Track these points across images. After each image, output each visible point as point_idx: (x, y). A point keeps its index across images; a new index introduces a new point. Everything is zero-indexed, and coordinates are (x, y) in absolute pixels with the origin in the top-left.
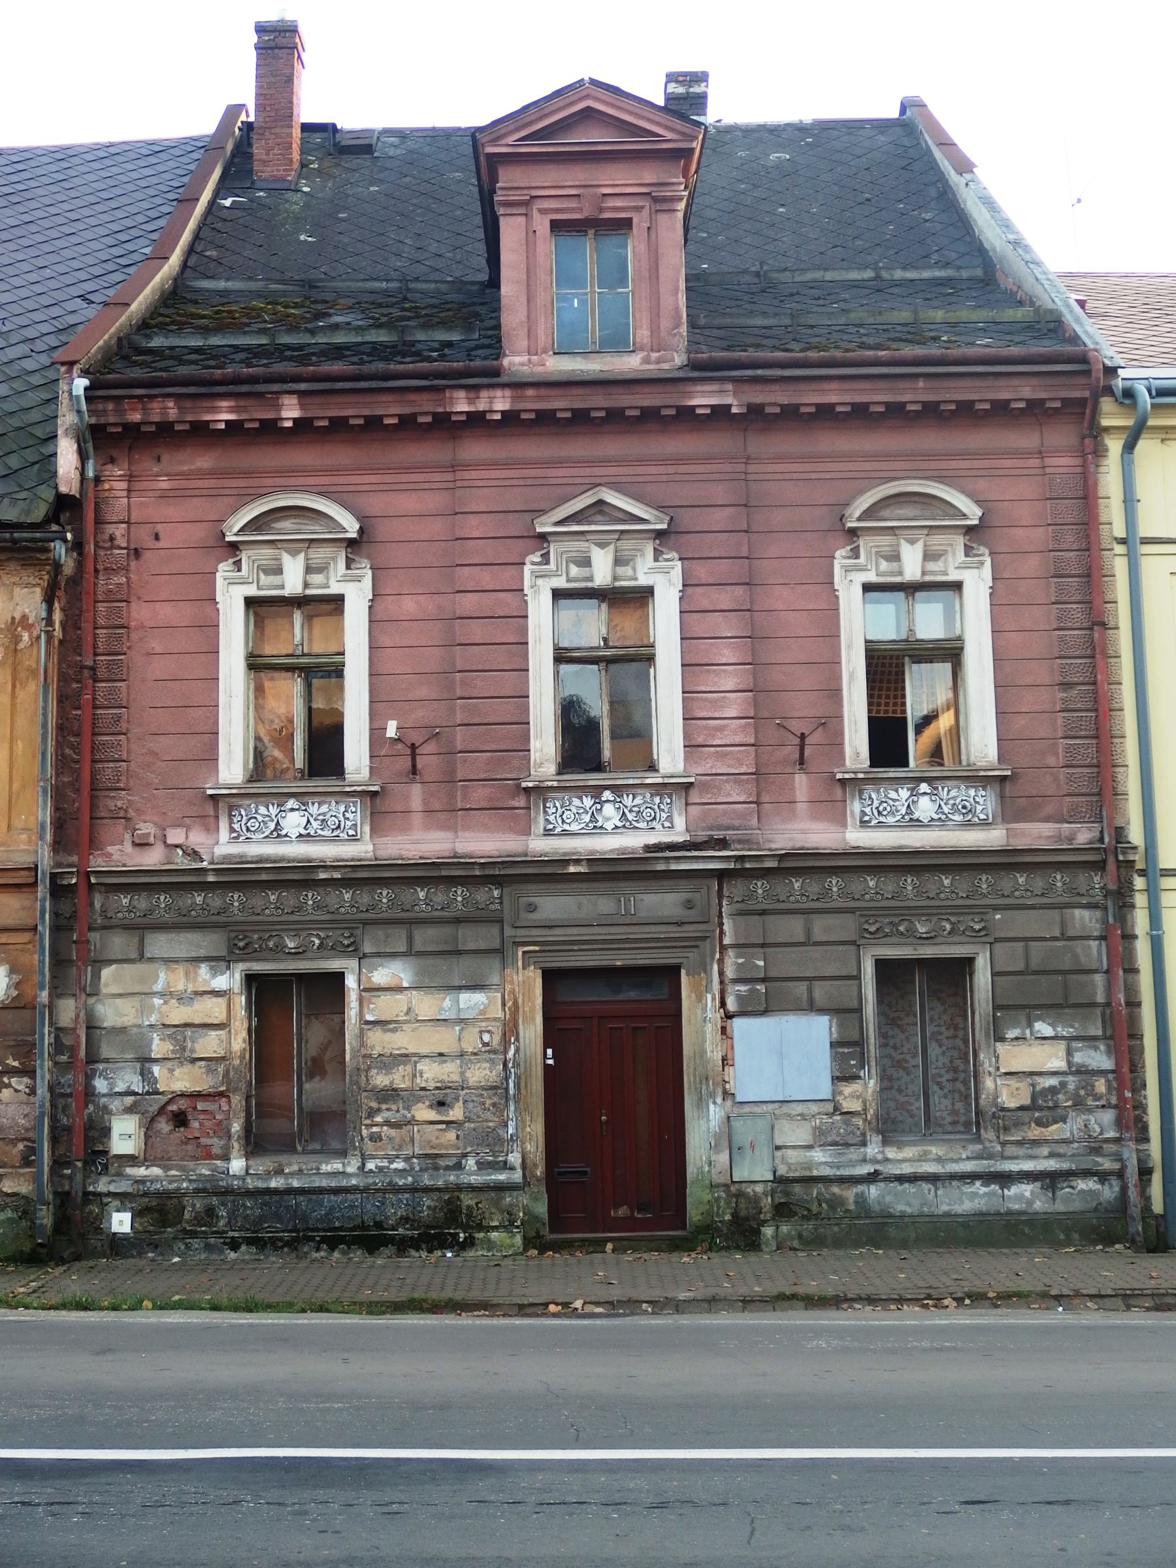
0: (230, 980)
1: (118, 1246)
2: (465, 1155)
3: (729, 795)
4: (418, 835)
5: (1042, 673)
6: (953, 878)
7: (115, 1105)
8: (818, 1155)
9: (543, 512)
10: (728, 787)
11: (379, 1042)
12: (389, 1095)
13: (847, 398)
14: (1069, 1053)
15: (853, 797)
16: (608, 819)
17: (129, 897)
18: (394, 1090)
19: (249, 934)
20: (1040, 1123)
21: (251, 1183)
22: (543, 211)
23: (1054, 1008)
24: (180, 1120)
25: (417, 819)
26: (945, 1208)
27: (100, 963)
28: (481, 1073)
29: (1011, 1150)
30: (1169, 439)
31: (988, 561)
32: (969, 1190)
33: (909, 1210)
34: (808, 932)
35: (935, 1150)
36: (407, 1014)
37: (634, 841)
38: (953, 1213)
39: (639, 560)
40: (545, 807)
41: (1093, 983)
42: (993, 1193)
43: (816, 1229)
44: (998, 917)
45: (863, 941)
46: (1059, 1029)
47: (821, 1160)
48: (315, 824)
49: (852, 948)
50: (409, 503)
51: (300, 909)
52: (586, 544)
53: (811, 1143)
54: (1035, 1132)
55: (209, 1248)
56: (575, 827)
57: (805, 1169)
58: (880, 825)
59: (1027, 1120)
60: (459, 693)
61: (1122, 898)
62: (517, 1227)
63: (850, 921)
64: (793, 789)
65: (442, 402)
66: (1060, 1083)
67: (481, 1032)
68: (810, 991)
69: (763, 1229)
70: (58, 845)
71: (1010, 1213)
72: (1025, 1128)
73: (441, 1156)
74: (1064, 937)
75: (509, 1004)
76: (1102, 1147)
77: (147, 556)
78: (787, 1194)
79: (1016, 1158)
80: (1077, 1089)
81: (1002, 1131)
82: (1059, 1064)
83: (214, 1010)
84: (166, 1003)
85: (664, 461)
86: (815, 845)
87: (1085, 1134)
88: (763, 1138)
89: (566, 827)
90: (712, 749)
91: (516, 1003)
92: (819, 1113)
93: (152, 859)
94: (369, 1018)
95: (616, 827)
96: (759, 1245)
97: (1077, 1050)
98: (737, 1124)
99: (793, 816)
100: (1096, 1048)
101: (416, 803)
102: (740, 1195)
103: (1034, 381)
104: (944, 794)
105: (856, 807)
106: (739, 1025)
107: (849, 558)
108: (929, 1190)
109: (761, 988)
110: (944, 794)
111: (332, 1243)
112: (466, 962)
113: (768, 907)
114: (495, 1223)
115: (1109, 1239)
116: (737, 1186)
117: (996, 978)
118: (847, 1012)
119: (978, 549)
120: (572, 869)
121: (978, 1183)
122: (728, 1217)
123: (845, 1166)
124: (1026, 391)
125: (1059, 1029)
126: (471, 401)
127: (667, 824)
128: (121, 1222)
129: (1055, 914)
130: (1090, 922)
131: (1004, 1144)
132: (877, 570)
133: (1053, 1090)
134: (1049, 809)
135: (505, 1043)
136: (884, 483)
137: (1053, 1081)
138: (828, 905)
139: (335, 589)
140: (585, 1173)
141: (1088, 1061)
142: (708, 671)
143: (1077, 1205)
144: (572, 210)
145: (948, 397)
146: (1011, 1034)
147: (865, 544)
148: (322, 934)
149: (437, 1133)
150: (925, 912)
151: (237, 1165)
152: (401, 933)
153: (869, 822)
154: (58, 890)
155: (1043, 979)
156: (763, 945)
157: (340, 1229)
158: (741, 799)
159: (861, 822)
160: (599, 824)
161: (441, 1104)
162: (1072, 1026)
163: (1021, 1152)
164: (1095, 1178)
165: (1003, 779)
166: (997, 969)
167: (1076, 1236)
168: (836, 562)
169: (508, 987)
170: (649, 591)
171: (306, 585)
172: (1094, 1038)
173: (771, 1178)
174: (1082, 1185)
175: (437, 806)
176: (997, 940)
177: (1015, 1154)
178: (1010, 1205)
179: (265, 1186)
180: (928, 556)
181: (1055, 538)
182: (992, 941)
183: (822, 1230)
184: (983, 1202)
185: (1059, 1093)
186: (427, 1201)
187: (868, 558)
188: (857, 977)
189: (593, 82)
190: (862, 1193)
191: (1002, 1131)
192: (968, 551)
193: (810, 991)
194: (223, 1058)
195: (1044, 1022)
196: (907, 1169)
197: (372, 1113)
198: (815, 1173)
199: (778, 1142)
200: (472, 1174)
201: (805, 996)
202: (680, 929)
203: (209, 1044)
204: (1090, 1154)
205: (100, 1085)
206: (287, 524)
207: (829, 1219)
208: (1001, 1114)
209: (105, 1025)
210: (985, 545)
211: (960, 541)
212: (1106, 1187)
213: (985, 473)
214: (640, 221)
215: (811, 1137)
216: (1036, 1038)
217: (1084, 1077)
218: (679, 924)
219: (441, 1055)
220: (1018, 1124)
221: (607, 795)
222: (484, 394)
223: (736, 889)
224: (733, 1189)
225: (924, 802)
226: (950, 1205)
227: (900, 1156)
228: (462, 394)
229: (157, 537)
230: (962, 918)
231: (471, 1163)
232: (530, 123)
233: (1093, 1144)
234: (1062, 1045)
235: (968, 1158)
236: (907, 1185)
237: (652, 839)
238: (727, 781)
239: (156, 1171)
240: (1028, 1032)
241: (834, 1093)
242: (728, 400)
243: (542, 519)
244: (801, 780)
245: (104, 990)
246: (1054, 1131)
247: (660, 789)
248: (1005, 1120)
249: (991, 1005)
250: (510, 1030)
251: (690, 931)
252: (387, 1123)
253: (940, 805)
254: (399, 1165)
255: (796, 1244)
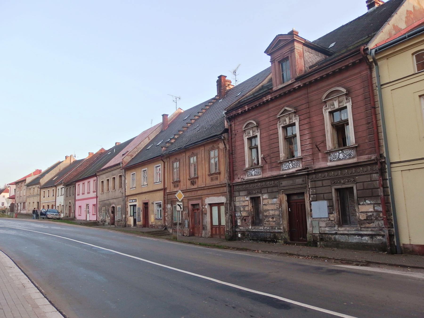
0: (248, 199)
1: (239, 239)
2: (276, 227)
3: (308, 159)
4: (268, 173)
5: (364, 122)
6: (348, 170)
7: (238, 218)
8: (327, 229)
9: (276, 115)
10: (308, 157)
11: (266, 208)
12: (266, 216)
13: (319, 76)
14: (374, 207)
15: (329, 156)
16: (290, 166)
17: (362, 168)
18: (267, 216)
19: (335, 180)
20: (369, 223)
21: (252, 230)
22: (276, 61)
23: (370, 197)
24: (245, 220)
25: (267, 170)
26: (350, 241)
27: (235, 197)
28: (277, 213)
29: (363, 229)
30: (388, 58)
31: (351, 100)
32: (355, 237)
33: (343, 241)
34: (323, 184)
35: (348, 229)
36: (268, 203)
37: (294, 170)
38: (352, 242)
39: (293, 118)
40: (282, 166)
41: (378, 191)
42: (360, 238)
43: (327, 244)
44: (357, 177)
45: (332, 185)
46: (371, 202)
47: (327, 230)
48: (256, 173)
49: (330, 187)
50: (264, 117)
51: (313, 178)
52: (285, 118)
53: (326, 226)
54: (368, 225)
55: (248, 240)
56: (286, 169)
57: (324, 231)
58: (334, 161)
59: (366, 223)
60: (271, 148)
61: (382, 172)
62: (283, 240)
63: (329, 181)
64: (319, 156)
65: (262, 100)
66: (372, 214)
67: (276, 206)
68: (324, 196)
69: (318, 243)
70: (230, 180)
71: (363, 243)
72: (366, 224)
73: (273, 227)
74: (371, 181)
75: (280, 201)
76: (382, 229)
77: (237, 135)
78: (322, 236)
79: (364, 231)
80: (376, 216)
81: (361, 225)
82: (372, 210)
83: (246, 203)
84: (242, 202)
85: (295, 99)
86: (322, 167)
87: (378, 226)
88: (317, 225)
89: (285, 169)
90: (305, 151)
91: (281, 200)
92: (327, 220)
93: (240, 180)
94: (263, 204)
95: (292, 168)
96: (317, 246)
97: (376, 206)
98: (313, 222)
99: (319, 162)
100: (380, 206)
101: (267, 168)
102: (314, 236)
103: (352, 58)
104: (255, 170)
105: (329, 158)
106: (312, 203)
107: (325, 107)
108: (347, 237)
109: (315, 196)
110: (345, 152)
111: (261, 240)
112: (274, 193)
113: (316, 180)
114: (280, 239)
115: (384, 251)
116: (314, 234)
117: (357, 191)
118: (330, 200)
119: (349, 98)
120: (284, 176)
121: (356, 236)
122: (312, 240)
123: (331, 231)
124: (351, 61)
125: (371, 202)
126: (266, 98)
127: (299, 166)
128: (239, 235)
129: (369, 176)
130: (377, 177)
131: (361, 228)
132: (283, 124)
133: (371, 215)
134: (367, 152)
135: (280, 207)
136: (325, 93)
137: (371, 214)
138: (326, 178)
139: (294, 122)
140: (295, 231)
141: (378, 209)
142: (304, 136)
143: (377, 242)
144: (280, 58)
145: (336, 68)
146: (361, 203)
147: (328, 104)
148: (348, 179)
149: (272, 223)
150: (343, 178)
151: (250, 227)
152: (266, 189)
153: (332, 160)
154: (230, 186)
155: (367, 191)
156: (315, 187)
157: (262, 238)
158: (310, 159)
159: (330, 161)
160: (289, 167)
161: (273, 218)
162: (374, 201)
163: (365, 229)
164: (381, 236)
165: (356, 147)
166: (357, 189)
167: (377, 249)
168: (323, 109)
169: (279, 198)
170: (295, 123)
171: (339, 106)
172: (379, 204)
173: (319, 233)
174: (378, 238)
175: (269, 168)
176: (357, 183)
177: (364, 230)
178: (363, 241)
179: (253, 231)
180: (339, 102)
181: (364, 91)
182: (356, 183)
183: (328, 244)
184: (358, 240)
185: (372, 216)
186: (272, 234)
187: (329, 106)
188: (331, 193)
189: (279, 35)
190: (335, 237)
191: (361, 225)
192: (347, 99)
193: (324, 196)
194: (248, 211)
195: (368, 200)
196: (342, 232)
197: (265, 219)
198: (326, 232)
199: (320, 226)
200: (276, 231)
201: (323, 197)
202: (302, 185)
203: (247, 209)
204: (379, 231)
205: (236, 215)
206: (250, 125)
207: (329, 242)
208: (361, 221)
209: (237, 206)
210: (350, 97)
211: (345, 97)
212: (384, 238)
213: (350, 81)
214: (289, 56)
215: (325, 225)
216: (367, 204)
217: (378, 213)
218: (302, 184)
219: (272, 210)
220: (364, 223)
221: (290, 162)
222: (267, 97)
223: (310, 177)
224: (313, 235)
225: (341, 155)
226: (351, 240)
227: (341, 229)
228: (264, 98)
229: (238, 132)
230: (349, 179)
231: (276, 228)
232: (272, 47)
233: (380, 228)
234: (372, 206)
235: (354, 231)
236: (343, 236)
237: (297, 169)
238: (308, 156)
239: (242, 228)
240: (365, 203)
241: (329, 216)
242: (300, 84)
243: (277, 115)
244: (320, 154)
245: (236, 201)
246: (372, 225)
247: (298, 159)
248: (361, 222)
249: (357, 197)
250: (280, 205)
251: (303, 186)
252: (267, 221)
253: (344, 155)
254: (268, 228)
255: (323, 246)
